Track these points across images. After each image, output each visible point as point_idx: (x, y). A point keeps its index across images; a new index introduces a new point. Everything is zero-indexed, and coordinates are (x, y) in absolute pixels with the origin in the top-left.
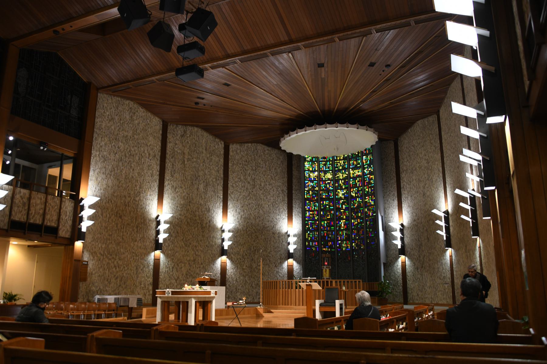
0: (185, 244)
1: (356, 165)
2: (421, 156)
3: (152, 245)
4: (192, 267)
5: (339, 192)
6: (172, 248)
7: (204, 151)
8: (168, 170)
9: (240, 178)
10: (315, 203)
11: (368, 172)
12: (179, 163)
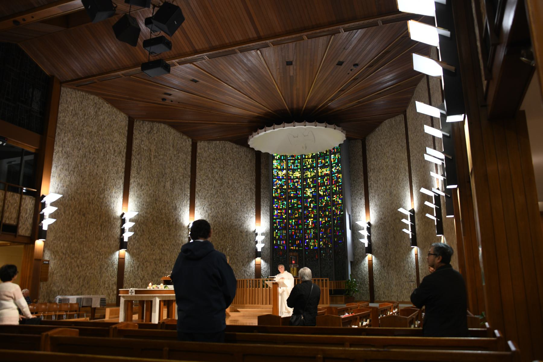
0: (151, 243)
1: (324, 164)
2: (388, 156)
3: (117, 244)
4: (158, 266)
5: (307, 190)
6: (137, 247)
7: (171, 148)
8: (134, 167)
9: (207, 176)
10: (283, 201)
11: (336, 171)
12: (145, 160)
